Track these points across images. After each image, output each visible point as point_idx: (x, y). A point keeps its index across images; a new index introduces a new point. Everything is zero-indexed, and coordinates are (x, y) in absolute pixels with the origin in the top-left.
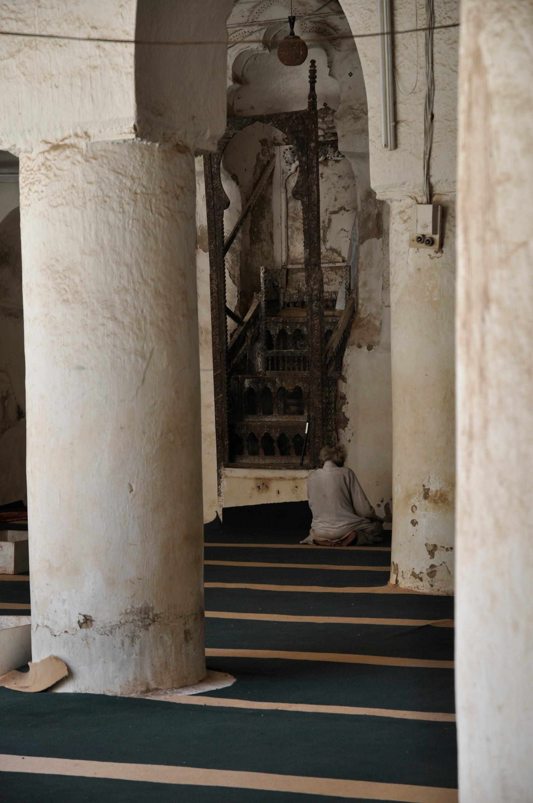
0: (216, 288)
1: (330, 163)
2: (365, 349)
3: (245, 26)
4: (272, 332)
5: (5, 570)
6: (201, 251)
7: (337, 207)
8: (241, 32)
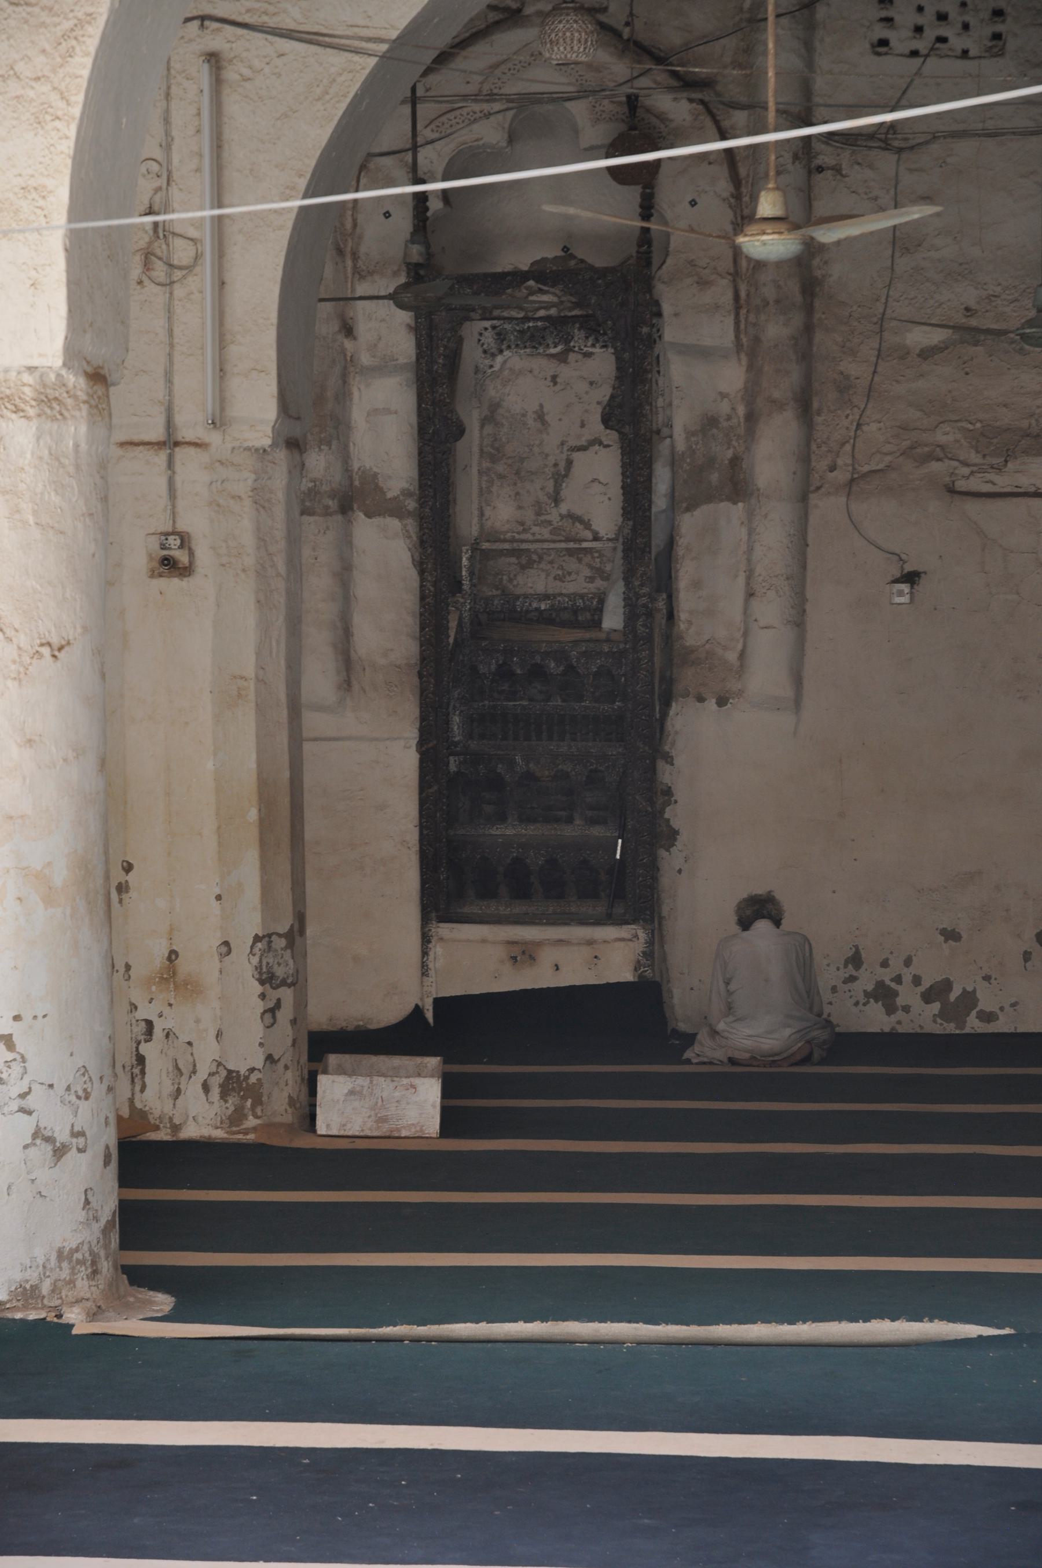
0: (432, 589)
1: (572, 357)
2: (711, 704)
3: (475, 101)
4: (483, 669)
5: (421, 1131)
6: (361, 515)
7: (584, 439)
8: (465, 111)
